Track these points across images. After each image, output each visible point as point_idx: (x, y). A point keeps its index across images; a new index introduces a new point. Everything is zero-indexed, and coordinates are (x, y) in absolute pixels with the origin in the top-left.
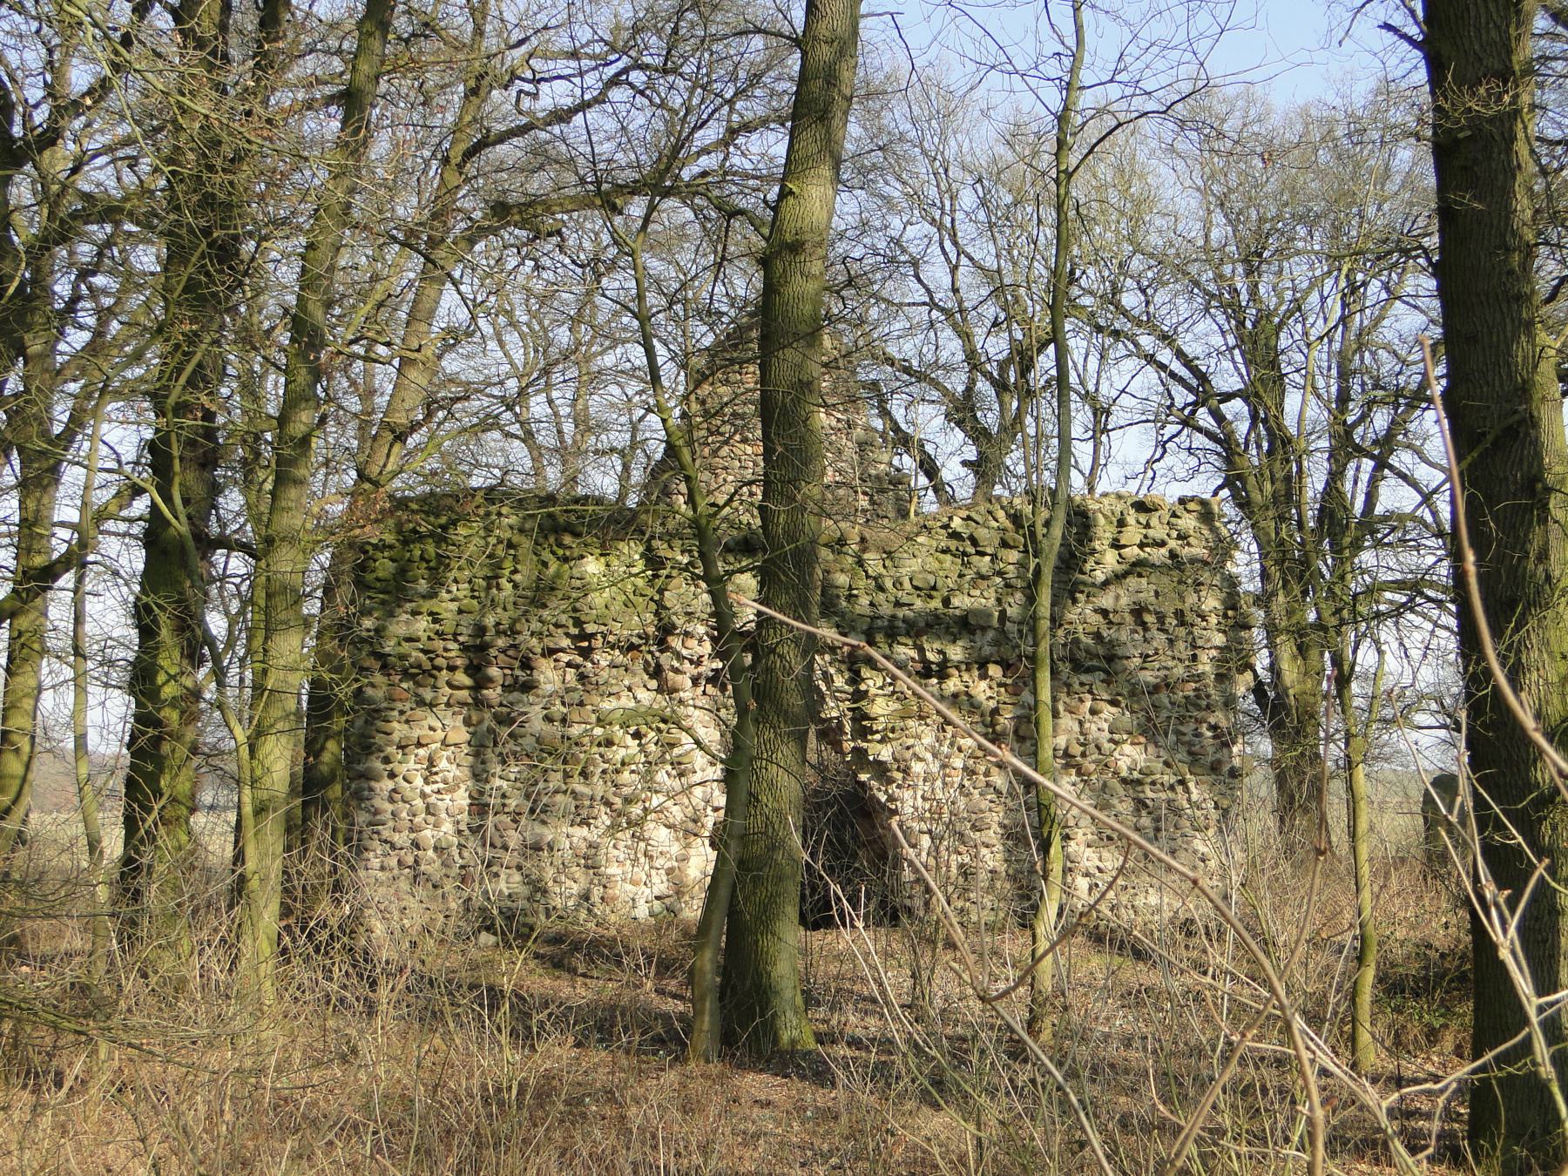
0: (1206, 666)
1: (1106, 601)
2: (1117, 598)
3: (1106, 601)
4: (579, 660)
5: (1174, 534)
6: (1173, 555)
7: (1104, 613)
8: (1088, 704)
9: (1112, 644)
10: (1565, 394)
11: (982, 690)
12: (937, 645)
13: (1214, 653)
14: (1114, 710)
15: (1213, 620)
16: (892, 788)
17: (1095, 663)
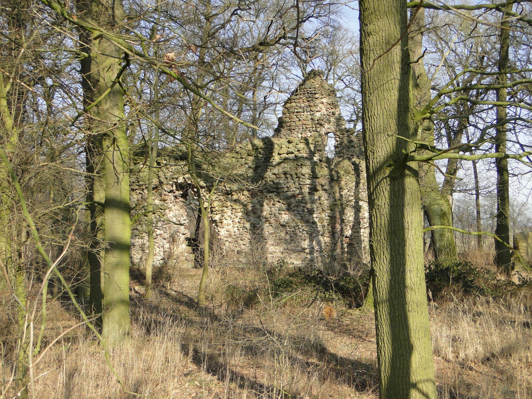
0: (306, 190)
1: (275, 171)
2: (278, 170)
3: (275, 171)
4: (142, 192)
5: (296, 150)
6: (296, 156)
7: (274, 174)
8: (272, 202)
9: (278, 183)
10: (99, 3)
11: (243, 198)
12: (229, 186)
13: (308, 186)
14: (279, 204)
15: (307, 176)
16: (219, 228)
17: (274, 190)
